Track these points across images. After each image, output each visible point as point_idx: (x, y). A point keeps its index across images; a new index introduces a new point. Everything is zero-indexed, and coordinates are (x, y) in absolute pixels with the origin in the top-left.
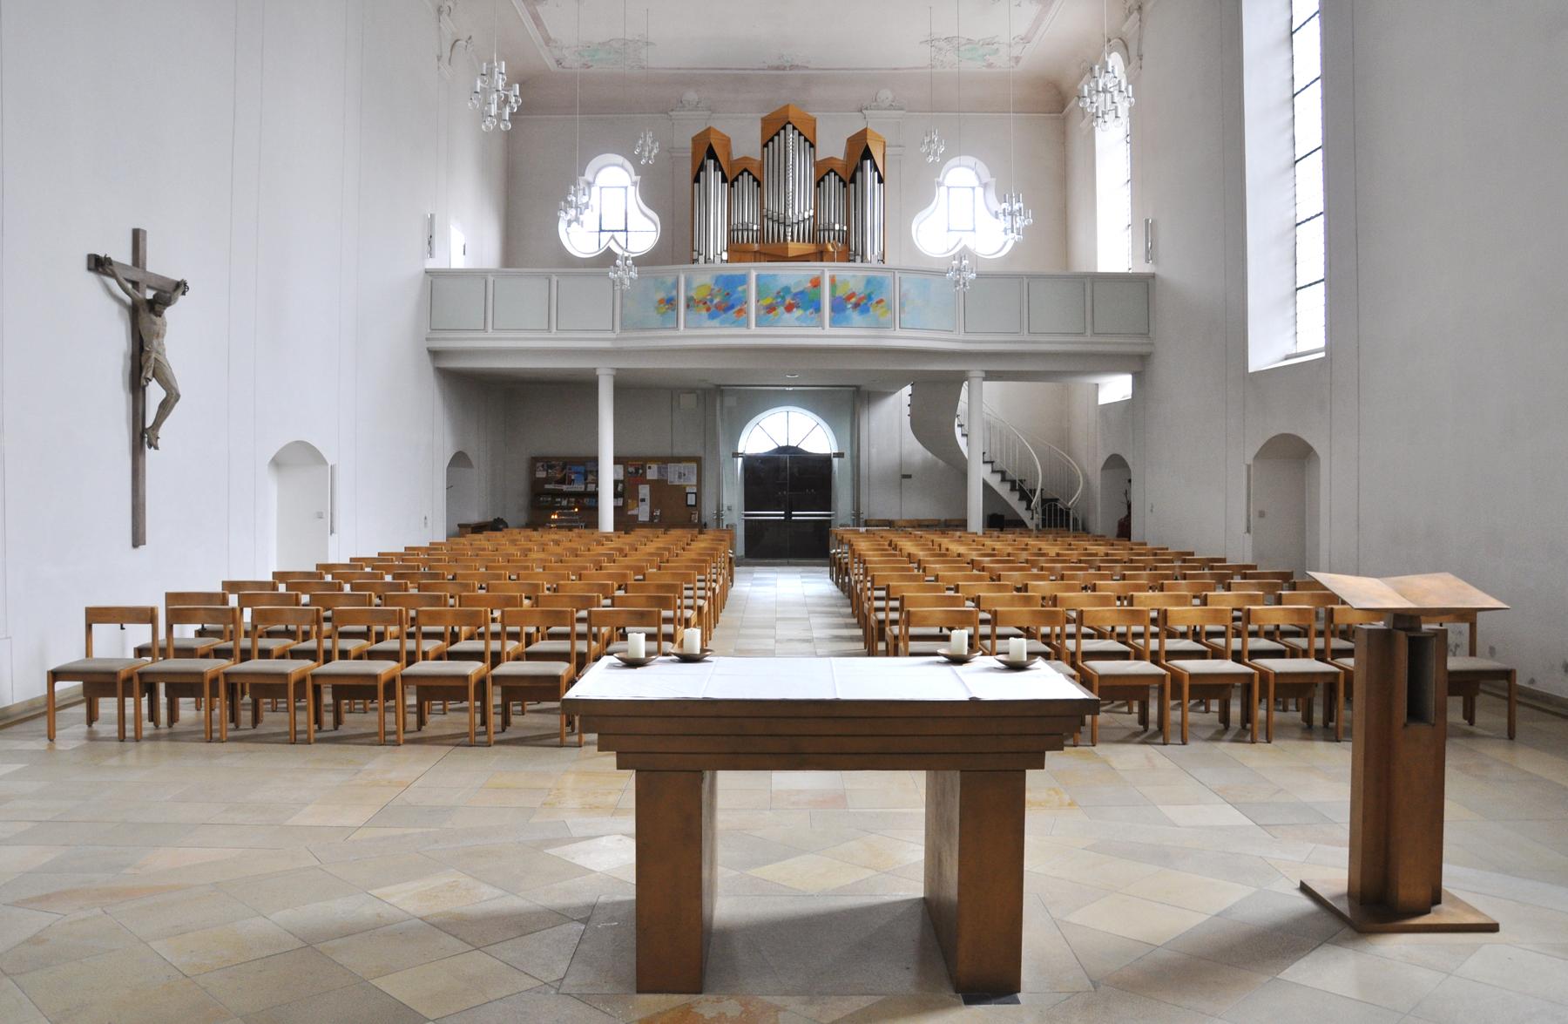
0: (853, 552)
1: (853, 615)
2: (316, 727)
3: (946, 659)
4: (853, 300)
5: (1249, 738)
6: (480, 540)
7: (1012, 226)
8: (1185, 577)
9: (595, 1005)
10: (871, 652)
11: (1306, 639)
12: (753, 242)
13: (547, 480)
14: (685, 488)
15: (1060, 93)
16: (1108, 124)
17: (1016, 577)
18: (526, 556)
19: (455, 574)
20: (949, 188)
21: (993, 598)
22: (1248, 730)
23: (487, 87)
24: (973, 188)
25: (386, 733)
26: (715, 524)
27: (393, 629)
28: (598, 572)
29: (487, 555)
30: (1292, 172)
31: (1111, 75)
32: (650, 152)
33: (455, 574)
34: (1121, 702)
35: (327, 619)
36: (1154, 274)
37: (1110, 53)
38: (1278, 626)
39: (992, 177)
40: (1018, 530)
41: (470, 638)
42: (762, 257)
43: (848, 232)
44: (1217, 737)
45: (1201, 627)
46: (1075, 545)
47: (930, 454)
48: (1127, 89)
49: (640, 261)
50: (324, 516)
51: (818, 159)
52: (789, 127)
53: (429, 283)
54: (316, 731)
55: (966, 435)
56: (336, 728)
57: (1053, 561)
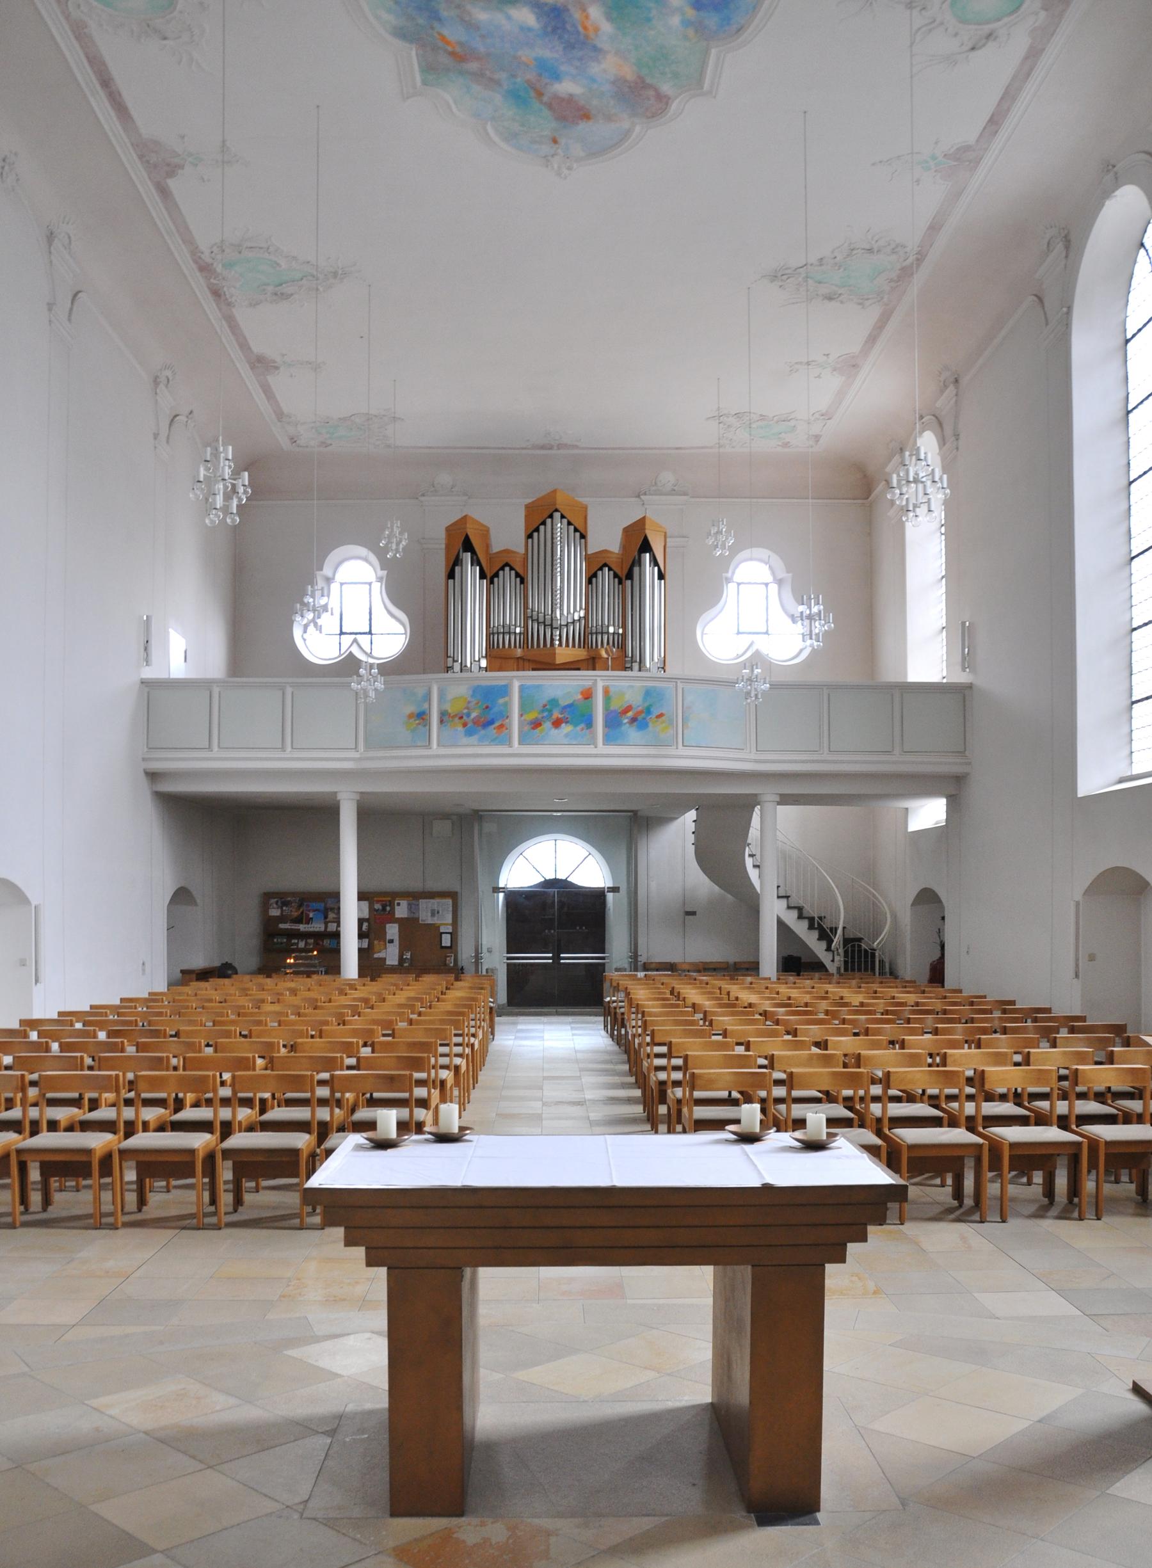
0: (630, 1001)
1: (631, 1073)
2: (22, 1208)
3: (735, 1137)
4: (630, 714)
5: (1076, 1214)
6: (206, 989)
7: (811, 631)
8: (1005, 1031)
9: (344, 1531)
10: (653, 1123)
11: (1141, 1102)
12: (515, 646)
13: (282, 919)
14: (439, 927)
15: (865, 476)
16: (920, 519)
17: (815, 1031)
18: (259, 1008)
19: (179, 1031)
20: (739, 584)
21: (788, 1057)
22: (1076, 1205)
23: (212, 475)
24: (767, 585)
25: (102, 1215)
26: (473, 969)
27: (109, 1096)
28: (341, 1027)
29: (212, 1008)
30: (1128, 570)
31: (924, 463)
32: (398, 544)
33: (179, 1031)
34: (931, 1174)
35: (33, 1084)
36: (971, 683)
37: (923, 431)
38: (1109, 1088)
39: (788, 572)
40: (817, 975)
41: (196, 1105)
42: (527, 664)
43: (624, 635)
44: (1040, 1213)
45: (1023, 1089)
46: (881, 992)
47: (716, 888)
48: (941, 479)
49: (389, 669)
50: (28, 963)
51: (589, 553)
52: (557, 515)
53: (146, 695)
54: (22, 1213)
55: (758, 866)
56: (45, 1209)
57: (857, 1012)
